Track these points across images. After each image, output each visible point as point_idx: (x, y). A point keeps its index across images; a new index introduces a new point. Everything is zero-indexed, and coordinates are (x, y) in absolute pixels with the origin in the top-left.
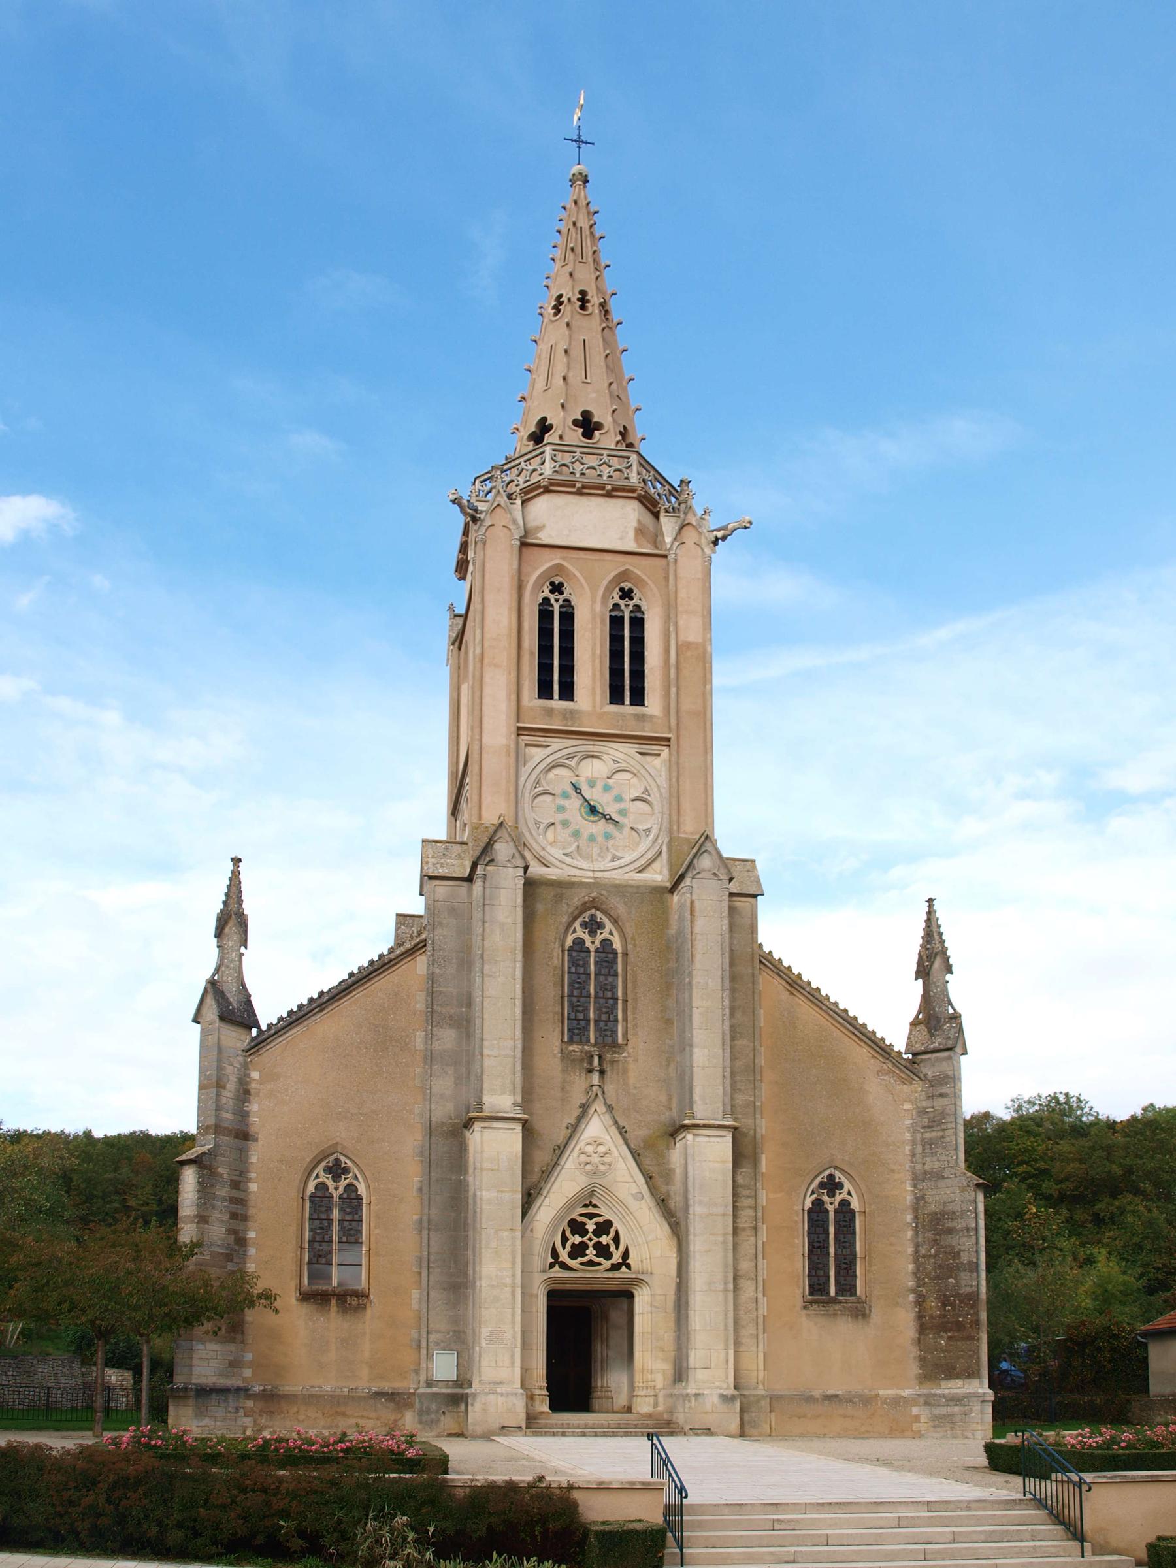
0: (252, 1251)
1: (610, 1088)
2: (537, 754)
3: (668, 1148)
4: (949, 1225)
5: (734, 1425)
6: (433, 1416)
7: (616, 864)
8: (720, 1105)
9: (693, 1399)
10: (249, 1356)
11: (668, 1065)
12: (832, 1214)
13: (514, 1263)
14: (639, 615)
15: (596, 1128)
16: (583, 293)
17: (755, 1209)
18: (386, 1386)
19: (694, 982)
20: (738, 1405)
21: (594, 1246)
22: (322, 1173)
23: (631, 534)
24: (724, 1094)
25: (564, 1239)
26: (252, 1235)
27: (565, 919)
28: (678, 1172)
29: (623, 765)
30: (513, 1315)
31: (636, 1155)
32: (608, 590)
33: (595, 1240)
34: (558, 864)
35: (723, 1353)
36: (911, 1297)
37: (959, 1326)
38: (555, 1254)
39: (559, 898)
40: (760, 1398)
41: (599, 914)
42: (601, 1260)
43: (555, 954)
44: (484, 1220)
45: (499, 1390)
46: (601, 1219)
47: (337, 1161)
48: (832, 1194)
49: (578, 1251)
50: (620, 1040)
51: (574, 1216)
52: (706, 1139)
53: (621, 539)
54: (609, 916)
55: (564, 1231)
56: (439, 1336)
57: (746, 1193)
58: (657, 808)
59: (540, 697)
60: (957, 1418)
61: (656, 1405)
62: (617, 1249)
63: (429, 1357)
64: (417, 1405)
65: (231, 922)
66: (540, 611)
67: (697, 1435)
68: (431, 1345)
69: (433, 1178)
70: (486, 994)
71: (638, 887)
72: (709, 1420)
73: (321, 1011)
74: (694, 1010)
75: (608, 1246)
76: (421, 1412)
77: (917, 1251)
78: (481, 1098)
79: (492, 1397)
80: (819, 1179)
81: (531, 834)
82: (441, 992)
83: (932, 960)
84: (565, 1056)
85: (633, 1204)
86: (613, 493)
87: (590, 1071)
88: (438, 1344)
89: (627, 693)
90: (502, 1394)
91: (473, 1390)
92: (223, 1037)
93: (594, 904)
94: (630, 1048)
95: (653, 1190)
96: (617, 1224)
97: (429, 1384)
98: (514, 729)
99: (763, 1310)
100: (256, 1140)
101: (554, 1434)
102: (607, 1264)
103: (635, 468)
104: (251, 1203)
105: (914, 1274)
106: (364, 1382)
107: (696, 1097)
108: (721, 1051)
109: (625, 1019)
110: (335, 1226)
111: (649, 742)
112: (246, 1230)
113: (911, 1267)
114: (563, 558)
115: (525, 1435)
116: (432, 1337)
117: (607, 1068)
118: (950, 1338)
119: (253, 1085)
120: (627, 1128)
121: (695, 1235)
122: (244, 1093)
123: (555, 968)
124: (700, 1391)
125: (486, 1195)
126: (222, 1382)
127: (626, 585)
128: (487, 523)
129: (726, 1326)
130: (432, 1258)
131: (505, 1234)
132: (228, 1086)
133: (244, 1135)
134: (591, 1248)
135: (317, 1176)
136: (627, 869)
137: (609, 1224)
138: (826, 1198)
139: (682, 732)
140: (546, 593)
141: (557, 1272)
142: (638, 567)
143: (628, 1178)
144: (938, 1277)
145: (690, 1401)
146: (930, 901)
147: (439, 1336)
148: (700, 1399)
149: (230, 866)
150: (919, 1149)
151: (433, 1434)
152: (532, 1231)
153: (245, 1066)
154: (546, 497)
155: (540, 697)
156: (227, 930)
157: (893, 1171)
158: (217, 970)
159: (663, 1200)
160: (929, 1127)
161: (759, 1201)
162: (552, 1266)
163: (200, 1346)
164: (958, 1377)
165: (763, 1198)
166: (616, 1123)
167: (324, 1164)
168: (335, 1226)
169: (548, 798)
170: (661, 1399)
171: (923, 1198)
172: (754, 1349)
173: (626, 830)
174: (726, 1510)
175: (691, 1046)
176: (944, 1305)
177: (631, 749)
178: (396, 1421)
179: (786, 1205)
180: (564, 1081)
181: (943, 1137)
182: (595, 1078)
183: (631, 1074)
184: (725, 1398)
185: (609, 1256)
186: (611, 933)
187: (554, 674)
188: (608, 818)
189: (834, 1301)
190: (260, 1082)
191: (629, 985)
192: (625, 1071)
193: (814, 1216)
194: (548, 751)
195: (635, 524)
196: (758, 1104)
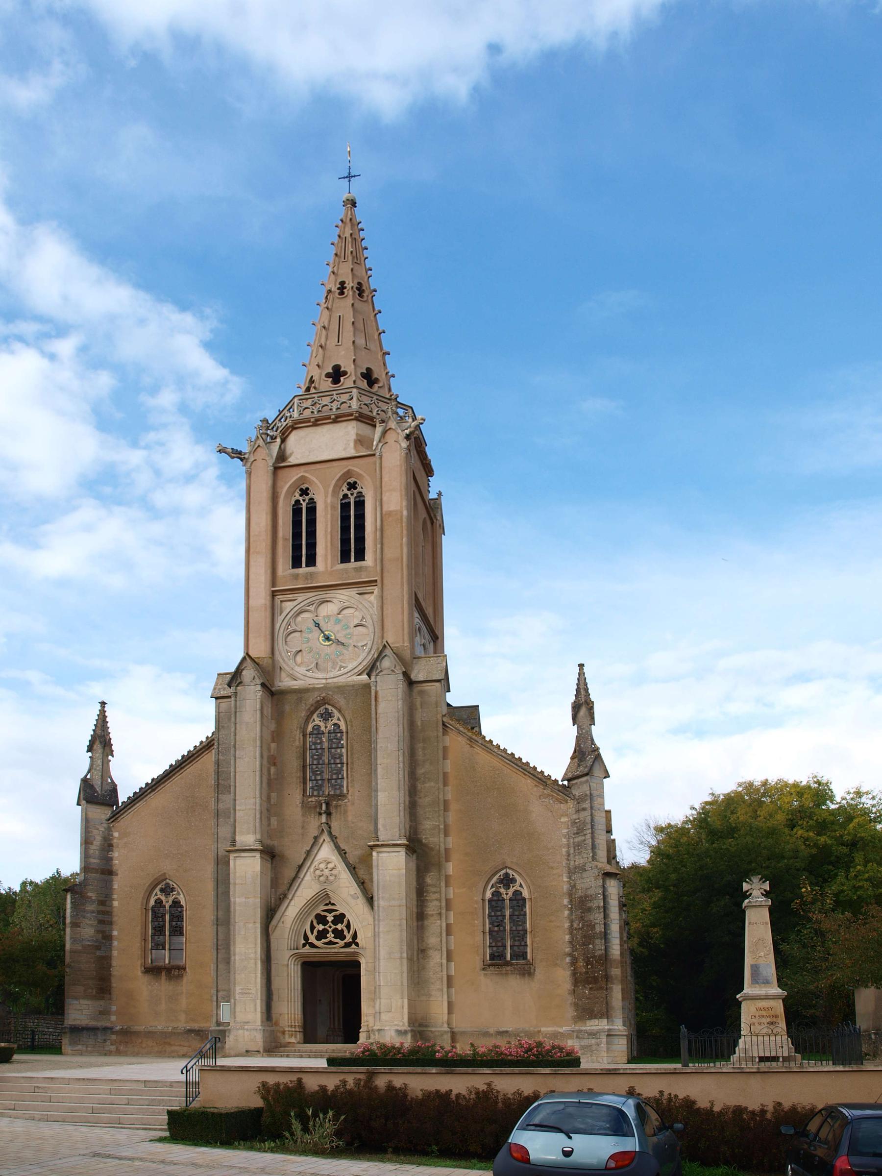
0: (115, 943)
1: (335, 825)
2: (288, 606)
4: (589, 905)
7: (343, 671)
8: (397, 829)
9: (377, 1033)
10: (114, 1008)
12: (507, 902)
14: (362, 499)
15: (326, 852)
16: (342, 283)
17: (440, 900)
18: (196, 1026)
21: (333, 932)
22: (159, 893)
23: (352, 444)
25: (312, 928)
26: (115, 933)
27: (303, 714)
29: (347, 604)
30: (256, 978)
32: (338, 486)
34: (302, 677)
36: (568, 959)
37: (595, 980)
39: (300, 700)
41: (330, 708)
42: (338, 940)
46: (337, 913)
47: (507, 874)
48: (507, 887)
49: (321, 935)
50: (345, 792)
52: (388, 854)
53: (345, 449)
54: (336, 708)
55: (312, 922)
58: (371, 629)
59: (293, 568)
60: (594, 1048)
63: (218, 1007)
65: (101, 741)
66: (293, 510)
69: (220, 892)
70: (237, 770)
71: (353, 686)
73: (154, 790)
77: (572, 926)
79: (241, 1032)
80: (497, 876)
81: (284, 660)
83: (583, 708)
86: (337, 420)
87: (320, 814)
89: (353, 554)
90: (247, 1030)
92: (89, 813)
93: (324, 702)
97: (218, 1024)
98: (269, 593)
100: (117, 875)
101: (281, 1056)
102: (342, 943)
103: (355, 399)
104: (114, 914)
105: (570, 942)
106: (182, 1024)
110: (507, 920)
111: (363, 585)
112: (111, 930)
113: (567, 937)
114: (305, 472)
116: (220, 994)
117: (333, 811)
118: (591, 988)
119: (115, 841)
120: (347, 850)
122: (108, 845)
123: (297, 747)
126: (93, 1023)
127: (351, 480)
128: (251, 459)
130: (219, 943)
131: (251, 925)
132: (95, 842)
133: (108, 872)
135: (156, 895)
136: (349, 674)
137: (343, 916)
138: (502, 890)
139: (385, 574)
140: (297, 496)
142: (356, 467)
144: (584, 944)
146: (581, 666)
148: (382, 1032)
149: (99, 707)
150: (572, 851)
153: (109, 829)
154: (294, 432)
155: (293, 568)
156: (95, 747)
157: (552, 868)
158: (89, 772)
160: (577, 833)
162: (304, 945)
163: (75, 1002)
164: (595, 1018)
167: (160, 886)
168: (507, 920)
169: (297, 634)
171: (575, 886)
173: (351, 648)
174: (23, 1081)
176: (587, 965)
177: (352, 592)
179: (463, 897)
180: (304, 822)
181: (585, 840)
182: (324, 818)
183: (349, 813)
185: (343, 937)
186: (339, 719)
187: (303, 552)
188: (338, 642)
189: (507, 964)
190: (120, 838)
192: (346, 812)
193: (494, 903)
194: (295, 603)
195: (354, 437)
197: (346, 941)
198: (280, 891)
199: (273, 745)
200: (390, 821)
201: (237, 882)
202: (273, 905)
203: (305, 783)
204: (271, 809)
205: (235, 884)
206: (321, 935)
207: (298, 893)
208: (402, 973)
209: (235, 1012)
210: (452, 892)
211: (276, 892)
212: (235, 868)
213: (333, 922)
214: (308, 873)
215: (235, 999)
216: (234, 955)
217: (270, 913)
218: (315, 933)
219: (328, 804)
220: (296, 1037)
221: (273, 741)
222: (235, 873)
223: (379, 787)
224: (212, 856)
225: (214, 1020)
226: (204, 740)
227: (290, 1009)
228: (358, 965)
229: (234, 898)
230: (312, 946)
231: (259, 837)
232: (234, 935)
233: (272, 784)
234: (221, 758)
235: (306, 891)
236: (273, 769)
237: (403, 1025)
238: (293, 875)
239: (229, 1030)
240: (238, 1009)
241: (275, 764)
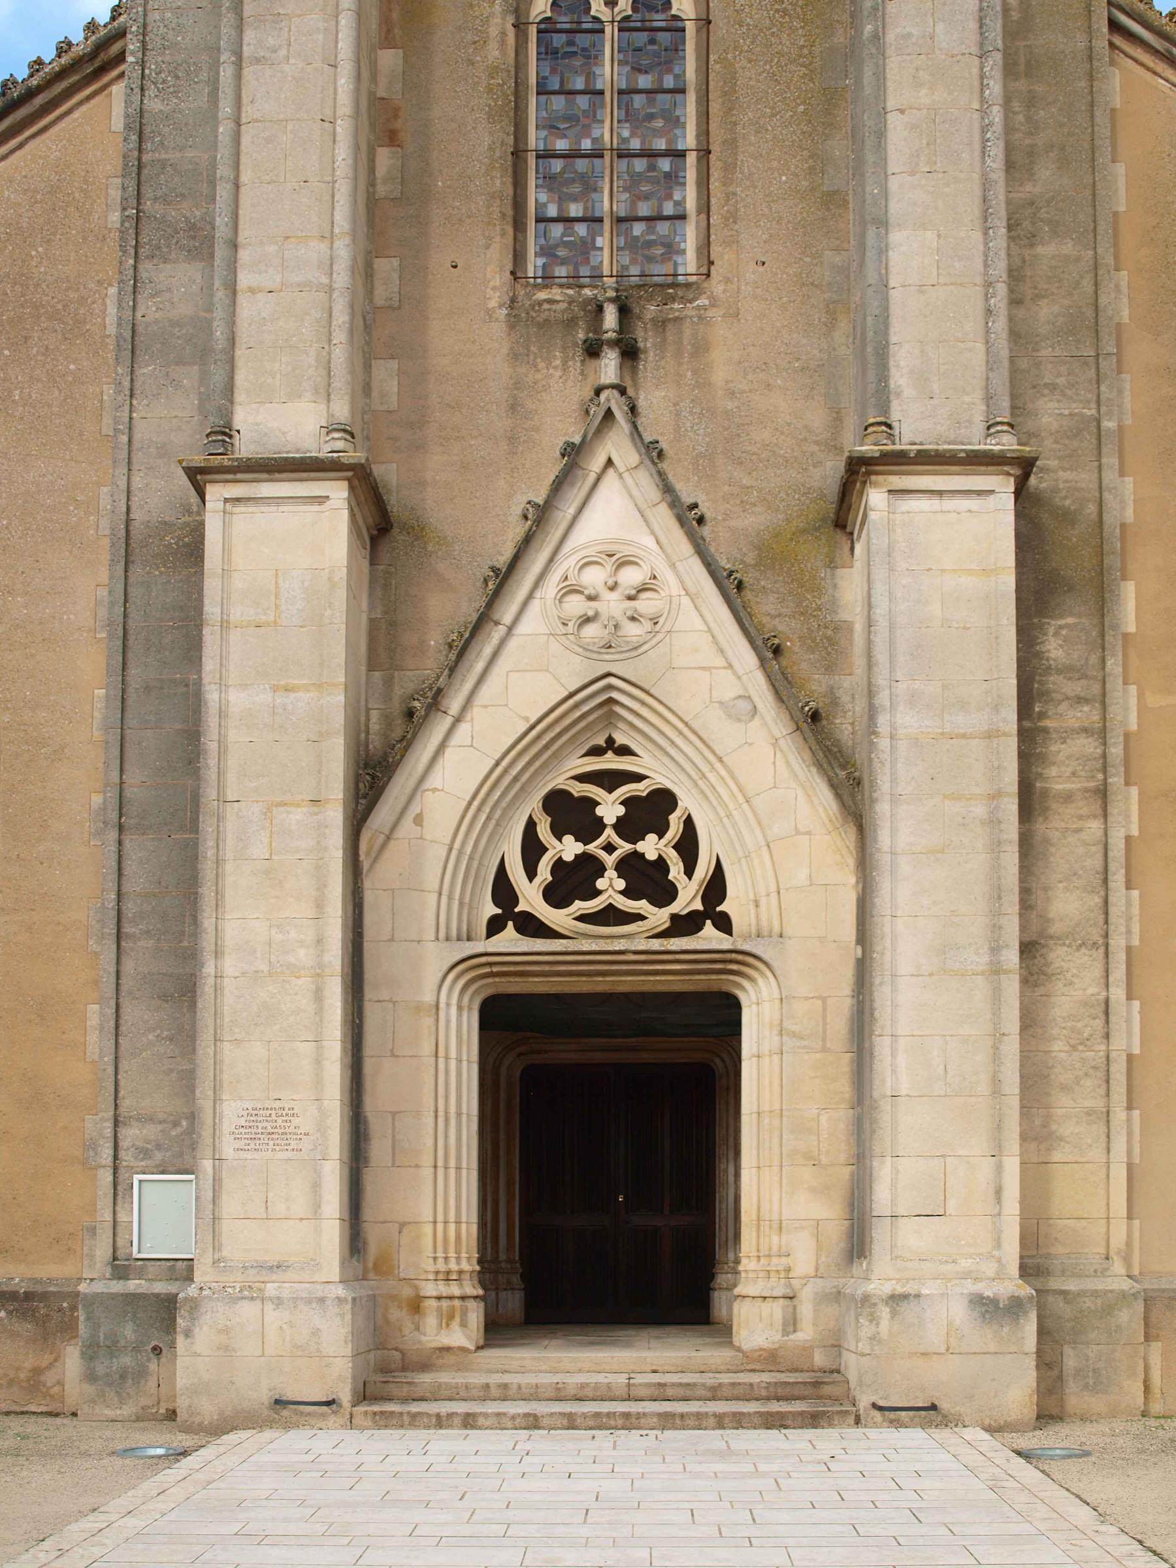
1: (654, 399)
3: (832, 564)
5: (1018, 1391)
6: (127, 1360)
9: (884, 1312)
11: (831, 325)
13: (320, 905)
15: (615, 514)
17: (1103, 734)
19: (890, 37)
20: (1030, 1327)
24: (990, 366)
25: (532, 849)
28: (859, 627)
30: (318, 1062)
31: (732, 588)
33: (624, 847)
35: (986, 1167)
38: (503, 891)
40: (1111, 1303)
43: (494, 32)
44: (231, 778)
45: (271, 1289)
46: (640, 789)
51: (561, 778)
55: (531, 825)
56: (151, 1131)
57: (1074, 688)
61: (791, 1323)
62: (689, 872)
63: (119, 1190)
64: (83, 1328)
67: (898, 1424)
68: (126, 1157)
69: (134, 684)
70: (248, 112)
72: (937, 1378)
74: (893, 119)
75: (661, 864)
76: (90, 1353)
78: (227, 415)
79: (248, 1310)
82: (164, 164)
84: (519, 314)
85: (724, 733)
87: (593, 351)
88: (145, 1153)
90: (278, 1302)
91: (192, 1291)
94: (716, 286)
95: (783, 686)
96: (688, 802)
97: (121, 1267)
99: (1128, 1035)
102: (659, 917)
107: (899, 379)
108: (977, 236)
109: (705, 207)
115: (351, 1423)
116: (131, 1135)
117: (646, 339)
120: (705, 508)
121: (895, 799)
123: (493, 72)
124: (910, 1288)
125: (237, 699)
129: (996, 1082)
130: (130, 908)
131: (296, 816)
134: (611, 873)
137: (664, 800)
141: (509, 939)
143: (709, 656)
145: (873, 1319)
147: (151, 1131)
148: (908, 1310)
151: (127, 1410)
152: (419, 820)
159: (815, 716)
161: (1114, 710)
162: (495, 926)
165: (1127, 706)
166: (667, 489)
170: (806, 1310)
172: (1098, 1154)
175: (883, 223)
178: (37, 1372)
180: (518, 385)
182: (609, 367)
184: (988, 1309)
185: (664, 894)
191: (715, 107)
192: (701, 348)
196: (1109, 424)
197: (677, 907)
198: (407, 682)
199: (389, 59)
200: (939, 364)
201: (237, 613)
202: (376, 743)
203: (519, 225)
204: (384, 325)
205: (225, 625)
206: (572, 882)
207: (487, 693)
208: (998, 1036)
209: (215, 1219)
210: (1133, 702)
211: (388, 683)
212: (227, 549)
213: (620, 826)
214: (535, 605)
215: (218, 1160)
216: (218, 954)
217: (373, 775)
218: (544, 872)
219: (624, 311)
220: (464, 1324)
221: (388, 41)
222: (226, 573)
223: (893, 207)
224: (101, 529)
225: (102, 1251)
226: (77, 36)
227: (441, 1202)
228: (724, 1015)
229: (223, 685)
230: (531, 926)
231: (342, 410)
232: (219, 862)
233: (391, 219)
234: (154, 105)
235: (520, 683)
236: (385, 158)
237: (999, 1277)
238: (469, 611)
239: (194, 1305)
240: (230, 1206)
241: (392, 138)
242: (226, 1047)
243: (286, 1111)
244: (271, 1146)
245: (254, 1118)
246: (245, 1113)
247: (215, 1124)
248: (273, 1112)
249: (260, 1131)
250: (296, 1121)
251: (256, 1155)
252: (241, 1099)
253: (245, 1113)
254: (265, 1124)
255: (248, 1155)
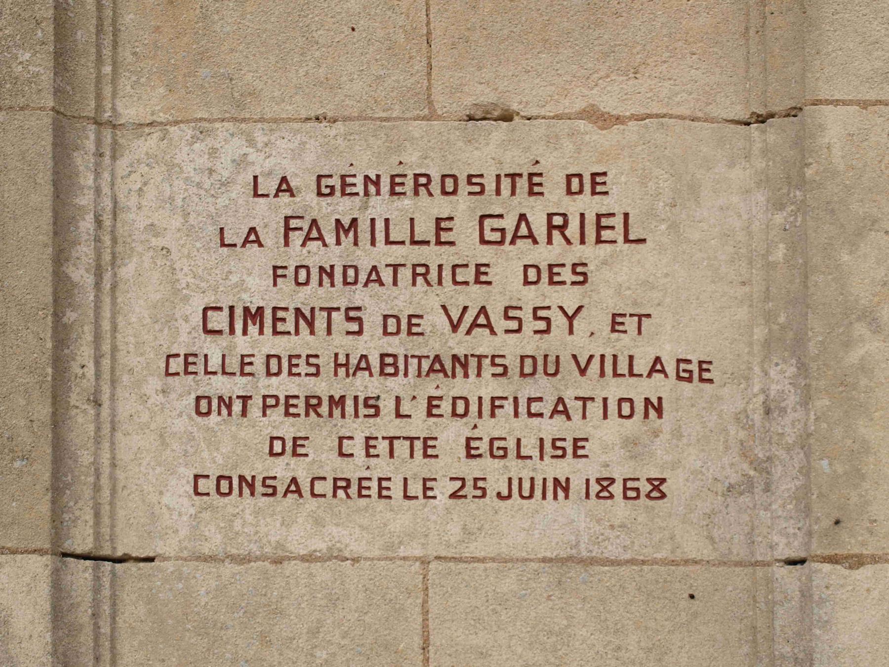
242: (119, 435)
243: (554, 197)
244: (450, 461)
245: (334, 255)
246: (267, 215)
247: (62, 292)
248: (462, 208)
249: (372, 344)
250: (618, 274)
251: (351, 528)
252: (240, 113)
253: (267, 215)
254: (404, 298)
255: (297, 527)
